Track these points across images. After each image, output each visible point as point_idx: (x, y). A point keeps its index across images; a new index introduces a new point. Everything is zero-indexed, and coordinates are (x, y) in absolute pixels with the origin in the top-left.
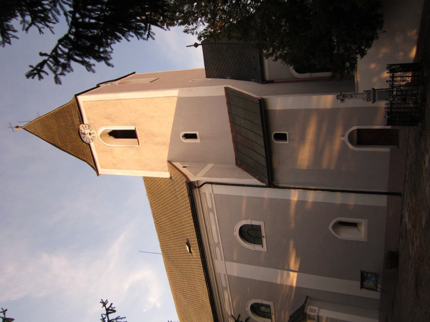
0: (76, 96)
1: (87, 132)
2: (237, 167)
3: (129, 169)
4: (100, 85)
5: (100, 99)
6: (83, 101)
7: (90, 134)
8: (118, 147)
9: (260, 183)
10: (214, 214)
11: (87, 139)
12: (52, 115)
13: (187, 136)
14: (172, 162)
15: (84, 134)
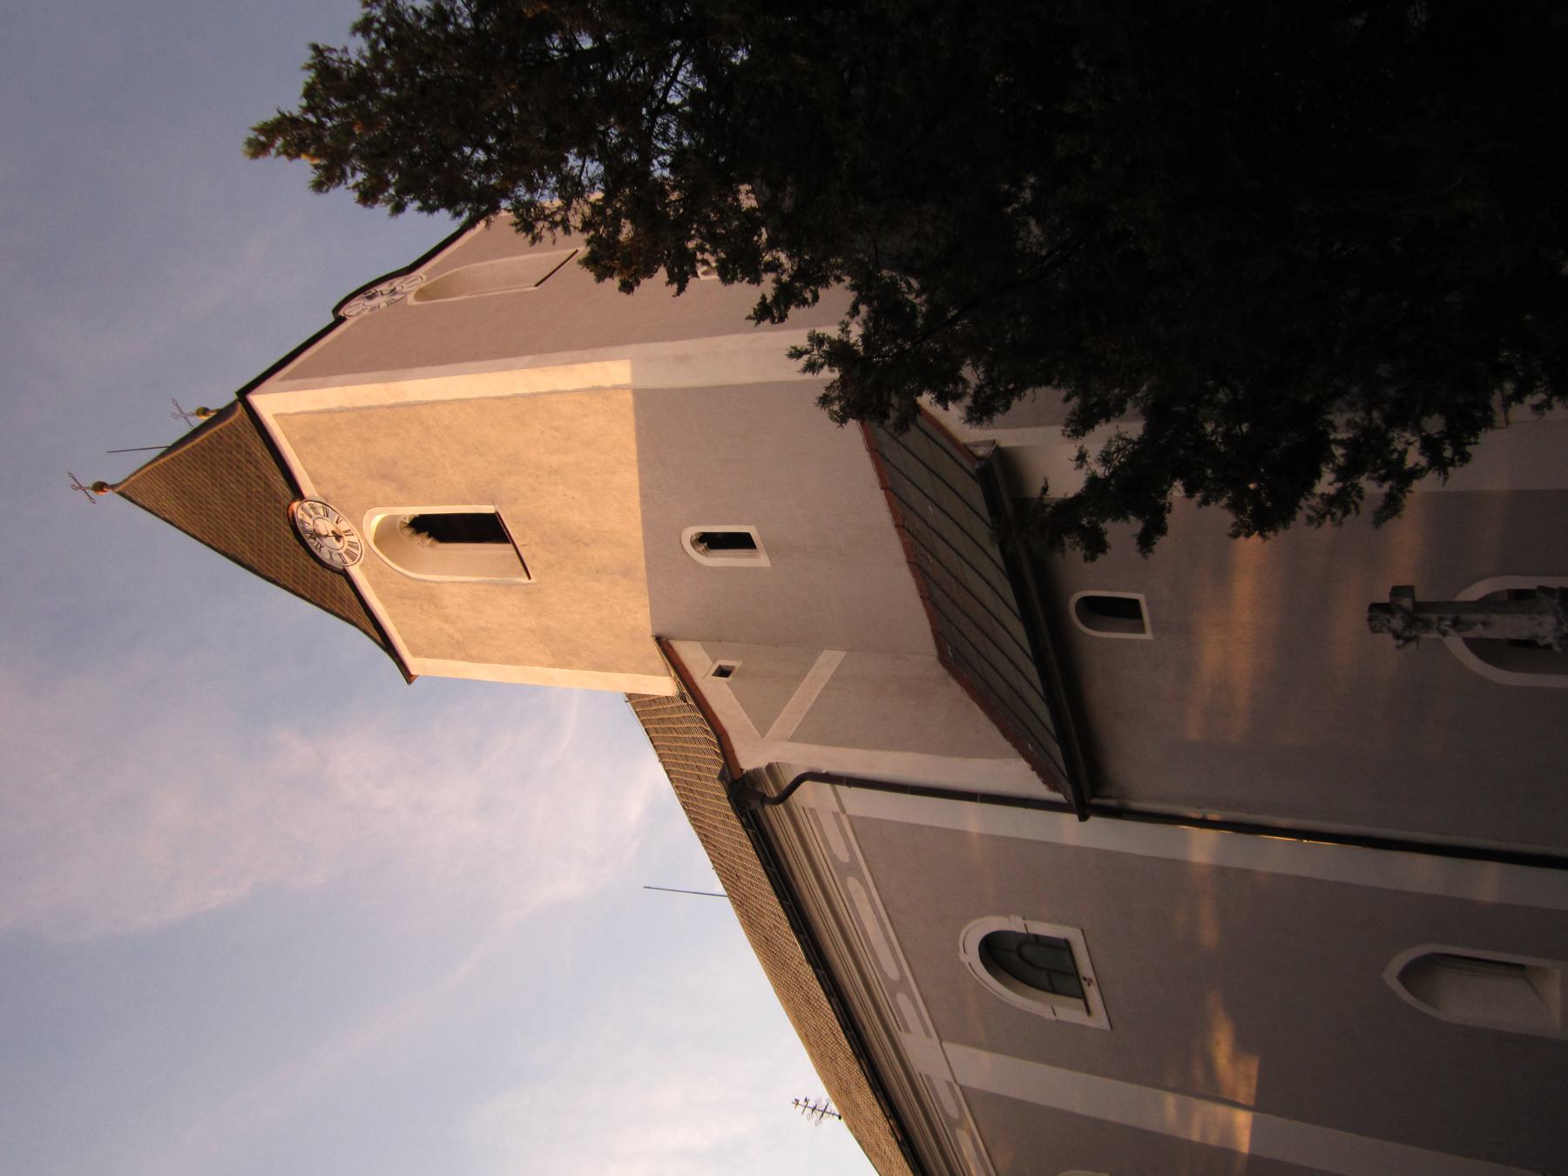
0: (243, 394)
1: (324, 526)
2: (944, 672)
3: (516, 661)
4: (341, 313)
5: (333, 405)
6: (276, 412)
7: (338, 538)
8: (453, 582)
9: (1040, 790)
10: (863, 882)
11: (331, 554)
12: (198, 448)
13: (712, 541)
14: (672, 639)
15: (316, 535)
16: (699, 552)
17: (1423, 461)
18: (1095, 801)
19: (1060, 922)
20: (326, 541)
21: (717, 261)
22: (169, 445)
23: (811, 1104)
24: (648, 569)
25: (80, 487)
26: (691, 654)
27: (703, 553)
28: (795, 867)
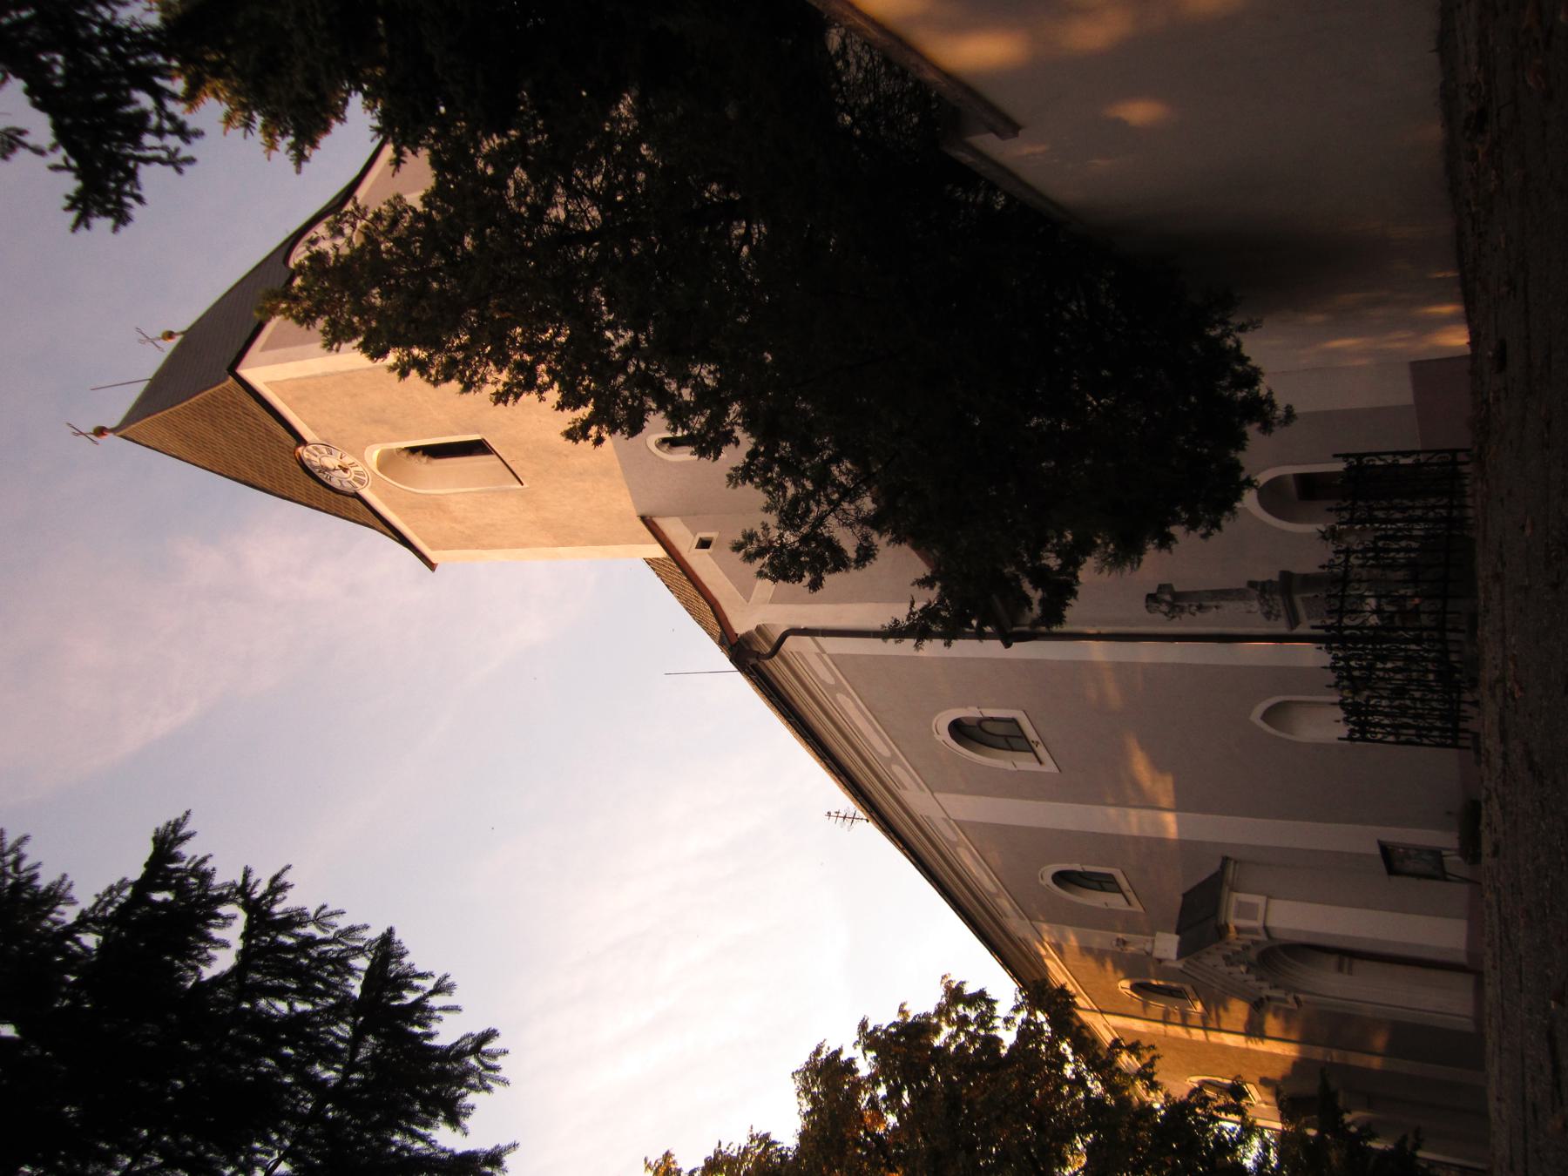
1: (331, 462)
5: (318, 371)
6: (266, 381)
7: (345, 470)
10: (848, 695)
11: (341, 482)
14: (655, 517)
16: (665, 452)
17: (1232, 338)
18: (1015, 629)
19: (1007, 708)
20: (335, 473)
21: (619, 108)
22: (151, 377)
23: (842, 814)
24: (623, 468)
25: (81, 433)
26: (673, 528)
27: (667, 452)
28: (794, 695)
